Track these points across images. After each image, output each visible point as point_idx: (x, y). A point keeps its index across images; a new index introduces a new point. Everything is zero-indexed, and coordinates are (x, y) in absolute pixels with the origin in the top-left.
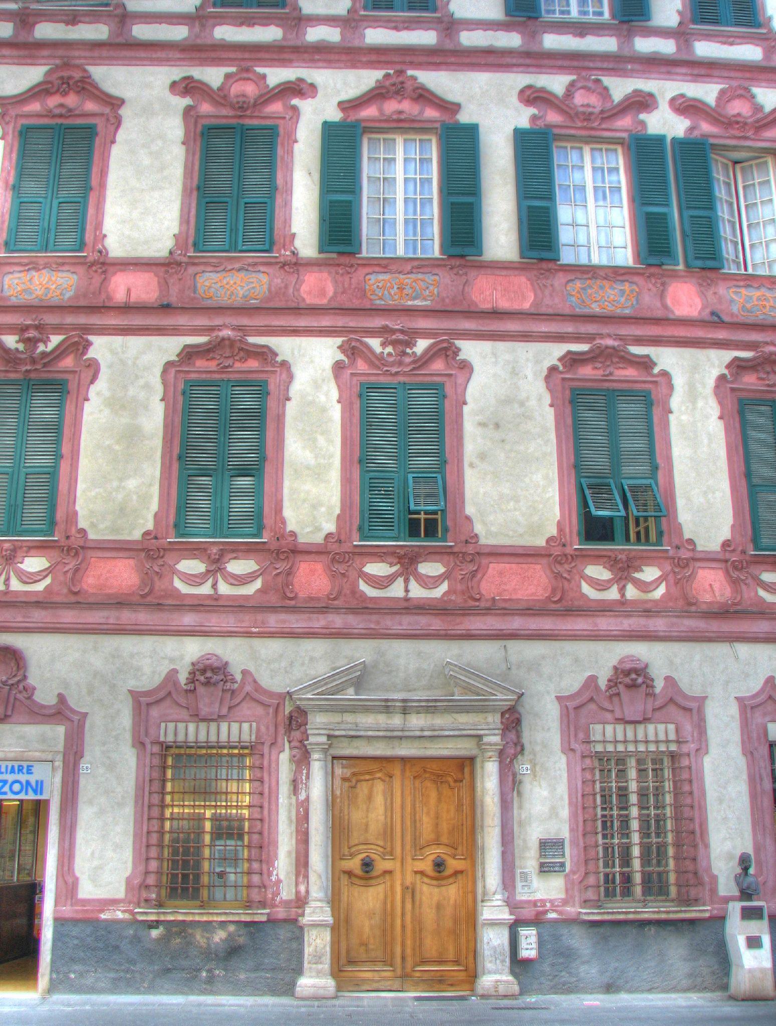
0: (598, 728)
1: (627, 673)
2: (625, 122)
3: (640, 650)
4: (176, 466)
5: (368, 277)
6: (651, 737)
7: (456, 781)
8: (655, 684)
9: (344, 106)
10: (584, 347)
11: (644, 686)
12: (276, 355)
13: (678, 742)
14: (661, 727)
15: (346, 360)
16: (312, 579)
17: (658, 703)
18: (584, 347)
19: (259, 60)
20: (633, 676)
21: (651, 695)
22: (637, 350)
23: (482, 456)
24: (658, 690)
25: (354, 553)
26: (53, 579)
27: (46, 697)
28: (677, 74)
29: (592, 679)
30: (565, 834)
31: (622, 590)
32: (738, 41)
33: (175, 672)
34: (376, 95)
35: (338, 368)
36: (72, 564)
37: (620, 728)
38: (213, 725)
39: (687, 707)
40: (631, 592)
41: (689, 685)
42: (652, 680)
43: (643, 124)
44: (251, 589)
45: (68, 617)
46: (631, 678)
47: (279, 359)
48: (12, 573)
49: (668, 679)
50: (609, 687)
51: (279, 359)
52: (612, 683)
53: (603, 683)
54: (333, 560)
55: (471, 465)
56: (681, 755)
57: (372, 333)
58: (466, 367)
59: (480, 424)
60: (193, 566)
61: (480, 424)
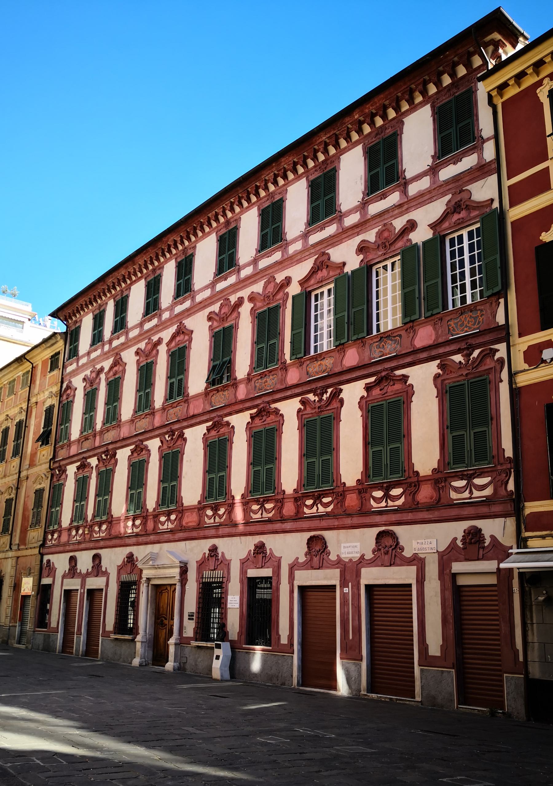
2: (400, 244)
5: (449, 323)
9: (433, 226)
10: (372, 379)
16: (190, 519)
18: (372, 379)
19: (276, 271)
22: (398, 372)
25: (303, 497)
26: (495, 490)
31: (471, 492)
32: (273, 253)
34: (313, 272)
36: (180, 515)
40: (321, 509)
43: (410, 240)
44: (329, 509)
45: (278, 526)
47: (280, 413)
48: (473, 489)
54: (436, 483)
57: (309, 392)
60: (379, 494)
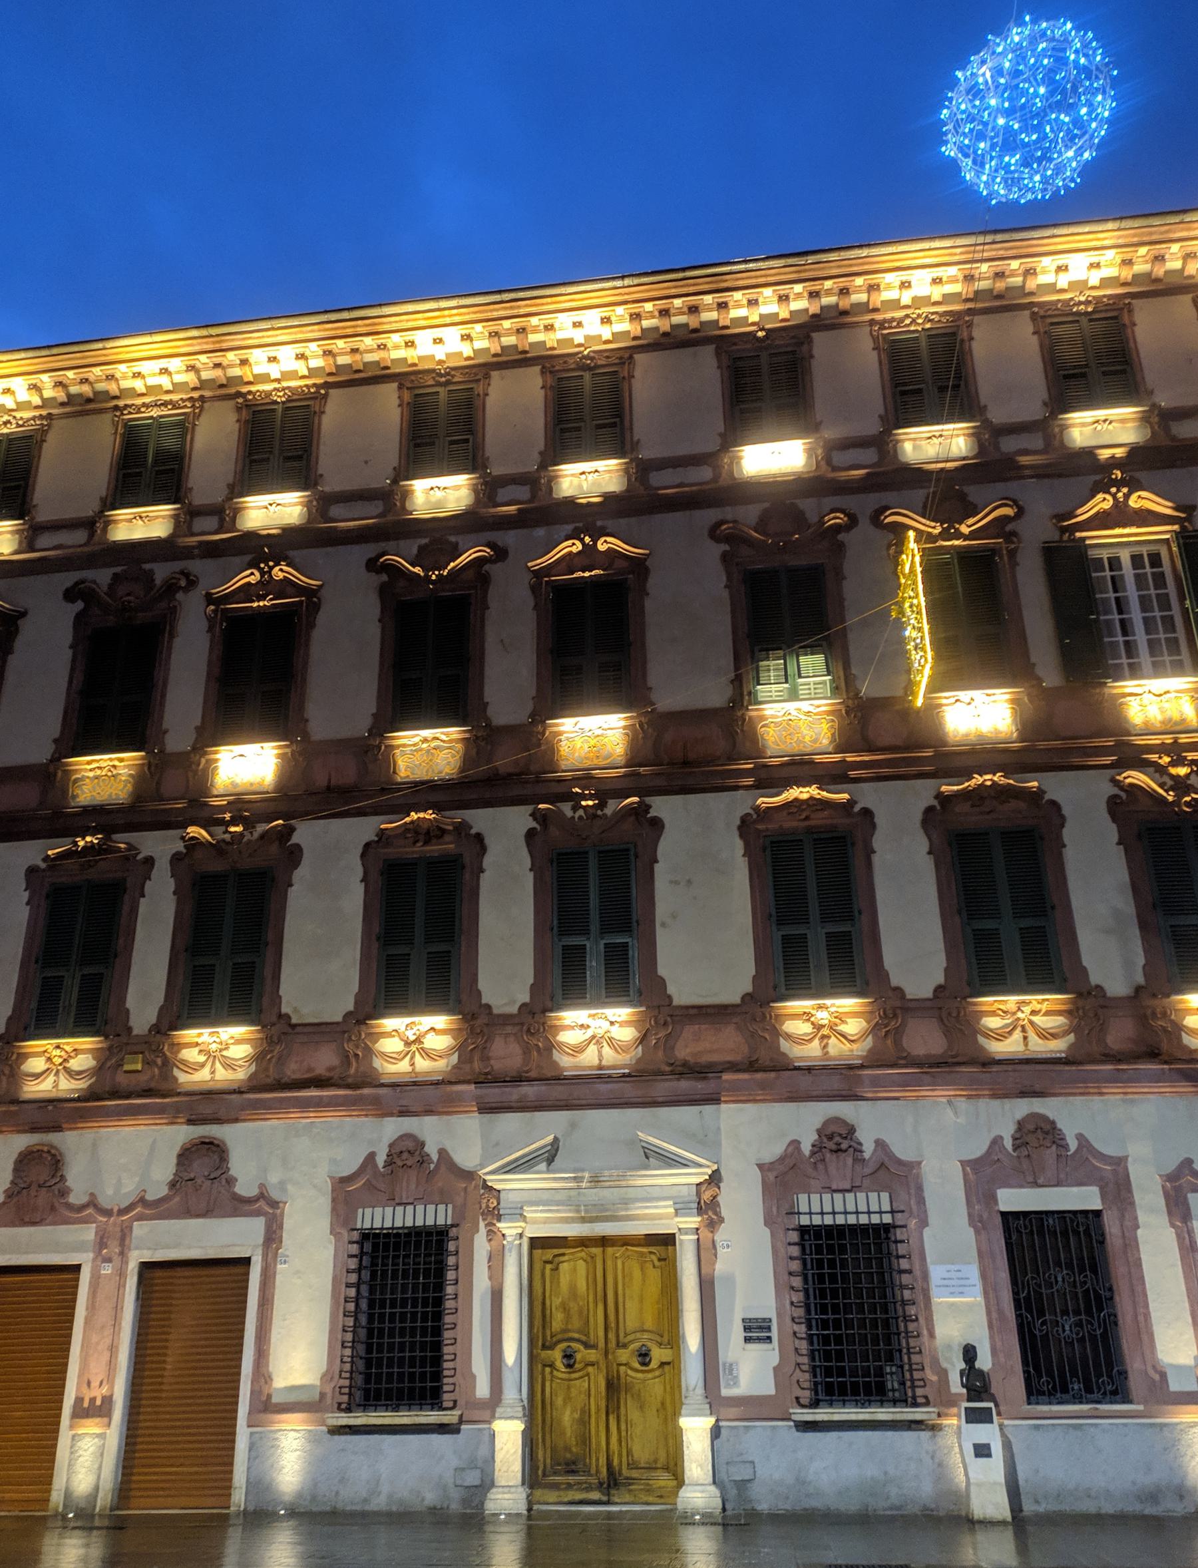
0: (803, 1198)
1: (830, 1137)
3: (409, 1125)
4: (375, 945)
6: (827, 1208)
7: (659, 1260)
8: (864, 1148)
11: (851, 1150)
12: (471, 828)
13: (892, 1212)
14: (873, 1196)
15: (538, 827)
17: (867, 1171)
20: (837, 1139)
21: (859, 1160)
23: (674, 916)
24: (867, 1155)
27: (245, 1187)
28: (244, 466)
29: (795, 1144)
30: (772, 1314)
33: (795, 1144)
35: (530, 835)
37: (827, 1197)
38: (410, 1208)
39: (894, 1173)
41: (902, 1150)
42: (860, 1144)
46: (407, 1155)
49: (1080, 1137)
50: (813, 1153)
51: (473, 831)
52: (817, 1148)
53: (806, 1148)
55: (663, 925)
56: (895, 1227)
58: (657, 825)
59: (671, 882)
61: (671, 882)
